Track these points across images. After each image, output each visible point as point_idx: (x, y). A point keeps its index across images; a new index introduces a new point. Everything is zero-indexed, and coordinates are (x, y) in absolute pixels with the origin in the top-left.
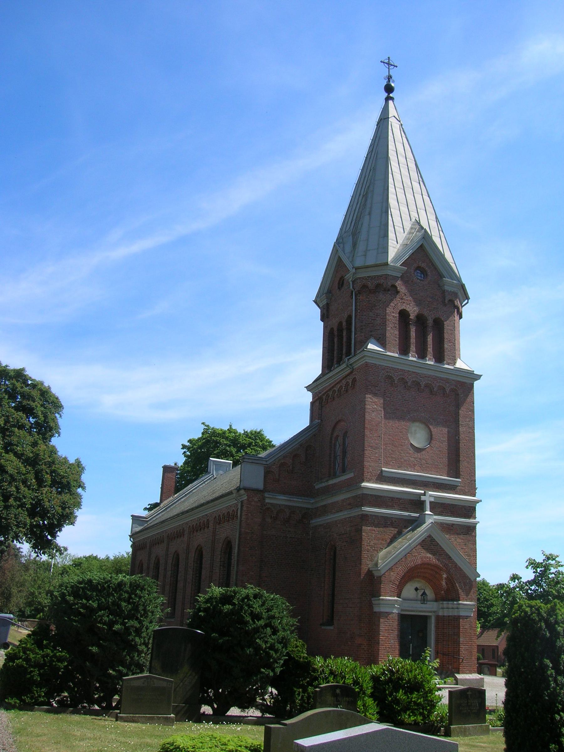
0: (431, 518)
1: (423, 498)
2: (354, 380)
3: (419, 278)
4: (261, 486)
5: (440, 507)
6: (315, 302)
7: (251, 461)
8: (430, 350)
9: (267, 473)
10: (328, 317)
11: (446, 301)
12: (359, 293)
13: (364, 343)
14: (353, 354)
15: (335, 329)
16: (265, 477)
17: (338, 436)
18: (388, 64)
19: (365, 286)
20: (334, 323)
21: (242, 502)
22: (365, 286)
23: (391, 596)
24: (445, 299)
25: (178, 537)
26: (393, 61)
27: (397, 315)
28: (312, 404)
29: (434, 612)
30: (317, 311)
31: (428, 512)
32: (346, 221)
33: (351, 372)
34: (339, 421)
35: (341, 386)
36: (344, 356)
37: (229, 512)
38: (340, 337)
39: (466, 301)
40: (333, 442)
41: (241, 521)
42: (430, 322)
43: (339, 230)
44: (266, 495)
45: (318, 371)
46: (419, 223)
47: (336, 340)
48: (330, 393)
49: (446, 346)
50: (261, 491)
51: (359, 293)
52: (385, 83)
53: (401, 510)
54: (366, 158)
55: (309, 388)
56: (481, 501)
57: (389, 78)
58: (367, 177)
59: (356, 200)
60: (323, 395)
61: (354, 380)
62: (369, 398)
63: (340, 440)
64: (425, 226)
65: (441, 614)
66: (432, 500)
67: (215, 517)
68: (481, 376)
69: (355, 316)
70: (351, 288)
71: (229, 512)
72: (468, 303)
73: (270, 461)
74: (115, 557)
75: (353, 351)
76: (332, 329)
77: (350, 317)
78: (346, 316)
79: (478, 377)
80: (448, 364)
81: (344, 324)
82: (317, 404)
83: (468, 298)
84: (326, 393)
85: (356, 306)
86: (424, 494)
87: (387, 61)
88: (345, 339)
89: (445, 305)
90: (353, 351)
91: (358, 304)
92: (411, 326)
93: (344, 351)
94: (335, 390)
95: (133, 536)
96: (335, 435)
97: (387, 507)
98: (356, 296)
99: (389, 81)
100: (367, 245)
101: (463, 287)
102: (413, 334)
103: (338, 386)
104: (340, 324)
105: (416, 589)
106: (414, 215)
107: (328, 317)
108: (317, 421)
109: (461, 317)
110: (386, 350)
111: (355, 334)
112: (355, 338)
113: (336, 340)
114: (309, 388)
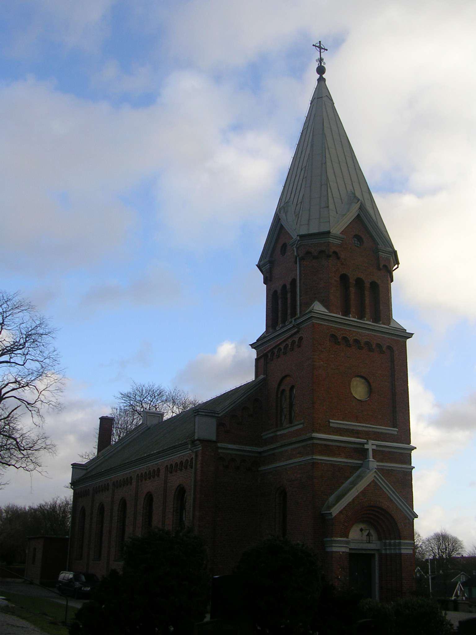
0: (373, 464)
1: (366, 446)
2: (301, 339)
4: (214, 438)
5: (380, 455)
6: (259, 266)
7: (203, 414)
8: (368, 311)
9: (220, 424)
10: (271, 281)
11: (381, 267)
12: (302, 259)
13: (309, 304)
15: (279, 291)
16: (217, 429)
17: (284, 390)
18: (320, 48)
19: (308, 253)
20: (278, 286)
21: (196, 452)
22: (308, 253)
23: (341, 537)
24: (379, 265)
25: (124, 485)
27: (338, 279)
28: (257, 360)
29: (378, 550)
30: (260, 277)
31: (371, 459)
32: (285, 193)
33: (297, 332)
34: (286, 376)
36: (289, 317)
37: (182, 461)
38: (285, 299)
39: (396, 266)
40: (279, 396)
41: (196, 470)
42: (367, 285)
44: (219, 445)
45: (264, 329)
49: (381, 307)
50: (214, 442)
51: (302, 259)
52: (316, 65)
53: (347, 458)
54: (302, 133)
55: (253, 346)
56: (416, 448)
57: (321, 60)
58: (304, 152)
59: (295, 172)
60: (268, 352)
61: (301, 339)
62: (232, 346)
63: (287, 393)
65: (383, 552)
66: (374, 447)
67: (167, 466)
69: (300, 280)
70: (295, 254)
71: (182, 461)
73: (222, 414)
74: (442, 539)
76: (275, 292)
77: (294, 282)
78: (290, 280)
81: (288, 287)
82: (262, 360)
86: (367, 443)
87: (318, 45)
89: (379, 269)
93: (289, 311)
94: (279, 348)
95: (74, 484)
96: (281, 388)
97: (334, 455)
98: (299, 262)
101: (395, 253)
102: (352, 296)
103: (290, 341)
104: (284, 286)
105: (361, 530)
106: (349, 187)
107: (271, 281)
108: (262, 377)
109: (392, 281)
111: (300, 296)
112: (300, 300)
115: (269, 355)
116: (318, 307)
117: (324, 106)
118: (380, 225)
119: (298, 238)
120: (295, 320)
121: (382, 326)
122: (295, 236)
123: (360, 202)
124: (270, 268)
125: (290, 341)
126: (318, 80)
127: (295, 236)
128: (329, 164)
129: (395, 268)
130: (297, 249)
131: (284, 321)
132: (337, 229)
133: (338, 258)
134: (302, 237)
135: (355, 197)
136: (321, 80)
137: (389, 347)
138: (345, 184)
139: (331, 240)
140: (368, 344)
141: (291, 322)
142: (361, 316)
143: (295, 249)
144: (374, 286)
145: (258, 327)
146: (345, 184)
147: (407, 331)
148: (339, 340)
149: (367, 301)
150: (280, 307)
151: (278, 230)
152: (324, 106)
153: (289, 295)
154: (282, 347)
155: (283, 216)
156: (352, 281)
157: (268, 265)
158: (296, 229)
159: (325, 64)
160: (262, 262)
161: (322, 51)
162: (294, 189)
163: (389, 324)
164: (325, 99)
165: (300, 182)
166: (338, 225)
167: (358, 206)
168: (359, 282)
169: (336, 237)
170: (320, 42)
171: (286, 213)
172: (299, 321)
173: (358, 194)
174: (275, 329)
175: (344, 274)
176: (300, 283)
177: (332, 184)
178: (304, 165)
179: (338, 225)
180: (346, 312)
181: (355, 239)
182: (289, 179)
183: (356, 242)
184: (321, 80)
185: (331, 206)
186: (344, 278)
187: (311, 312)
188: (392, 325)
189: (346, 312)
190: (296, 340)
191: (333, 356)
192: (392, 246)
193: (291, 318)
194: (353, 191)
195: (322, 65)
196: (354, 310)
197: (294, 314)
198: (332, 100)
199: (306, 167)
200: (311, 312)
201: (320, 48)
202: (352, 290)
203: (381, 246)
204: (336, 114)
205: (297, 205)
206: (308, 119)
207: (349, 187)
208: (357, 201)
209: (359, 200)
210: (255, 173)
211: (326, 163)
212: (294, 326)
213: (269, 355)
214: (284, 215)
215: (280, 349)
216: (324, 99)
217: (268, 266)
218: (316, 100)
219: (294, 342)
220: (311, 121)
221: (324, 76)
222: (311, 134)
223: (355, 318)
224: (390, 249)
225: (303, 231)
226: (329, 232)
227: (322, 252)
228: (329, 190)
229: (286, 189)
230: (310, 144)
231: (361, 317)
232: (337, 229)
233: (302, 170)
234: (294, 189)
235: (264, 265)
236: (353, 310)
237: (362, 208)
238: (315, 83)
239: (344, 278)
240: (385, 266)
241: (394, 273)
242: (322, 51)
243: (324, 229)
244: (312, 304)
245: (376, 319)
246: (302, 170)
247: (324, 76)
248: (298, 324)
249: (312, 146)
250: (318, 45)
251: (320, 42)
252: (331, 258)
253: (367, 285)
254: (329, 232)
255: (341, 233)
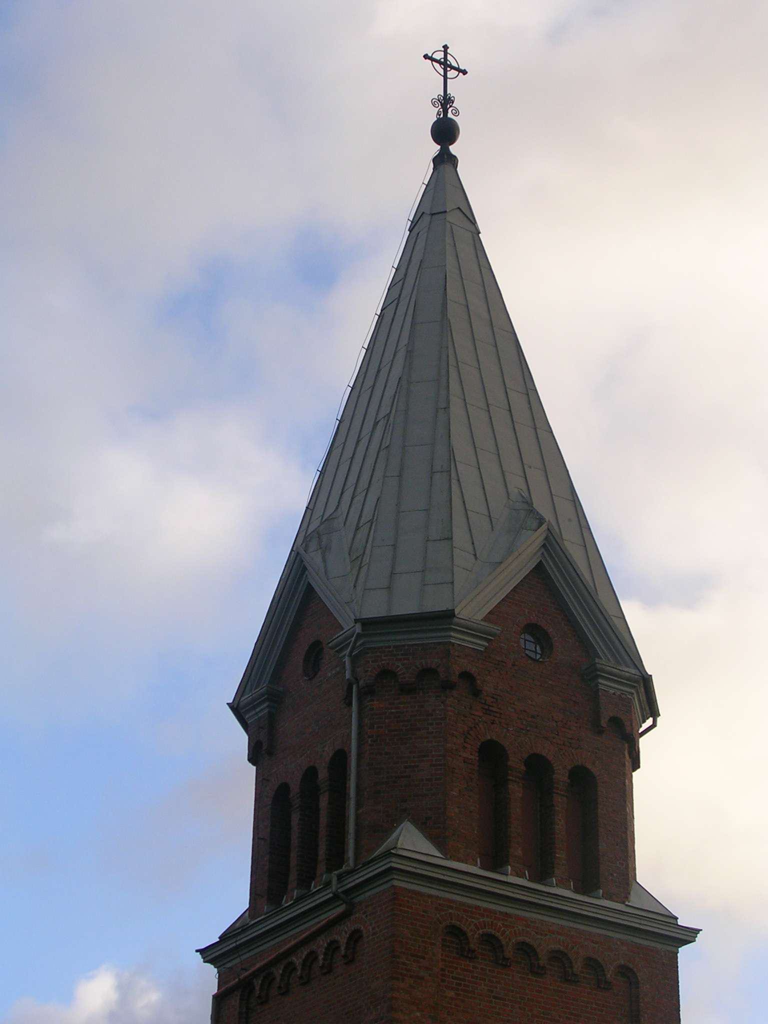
2: (356, 937)
3: (532, 655)
6: (236, 708)
8: (561, 855)
10: (270, 753)
11: (604, 723)
12: (367, 692)
13: (384, 828)
14: (351, 862)
18: (445, 64)
22: (385, 673)
26: (457, 56)
27: (474, 757)
28: (219, 1000)
30: (240, 739)
35: (312, 953)
36: (322, 867)
39: (650, 722)
43: (650, 668)
45: (243, 904)
46: (529, 503)
47: (295, 818)
48: (278, 971)
49: (602, 846)
51: (367, 692)
52: (432, 115)
55: (208, 954)
57: (446, 101)
60: (255, 975)
61: (356, 937)
64: (547, 515)
68: (697, 931)
70: (348, 675)
72: (654, 725)
75: (351, 854)
76: (284, 789)
77: (340, 759)
78: (328, 752)
79: (690, 935)
80: (608, 896)
82: (235, 1001)
83: (654, 712)
84: (260, 970)
85: (360, 726)
87: (439, 56)
88: (324, 819)
89: (600, 731)
90: (351, 854)
91: (366, 721)
92: (512, 786)
94: (291, 963)
99: (446, 112)
100: (394, 558)
101: (646, 682)
102: (516, 810)
103: (322, 943)
104: (311, 774)
106: (516, 483)
107: (270, 753)
109: (636, 765)
110: (445, 854)
111: (358, 805)
112: (357, 817)
113: (295, 818)
114: (208, 954)
115: (257, 983)
116: (411, 840)
117: (448, 240)
118: (603, 597)
119: (358, 628)
120: (340, 878)
121: (601, 904)
122: (348, 624)
123: (544, 527)
124: (271, 715)
125: (322, 943)
126: (434, 160)
127: (348, 624)
128: (456, 409)
129: (645, 726)
130: (354, 660)
131: (306, 879)
132: (473, 607)
133: (476, 693)
134: (368, 624)
135: (531, 511)
136: (445, 161)
137: (625, 972)
138: (503, 472)
139: (456, 638)
140: (558, 957)
141: (328, 884)
142: (542, 872)
143: (347, 660)
144: (582, 779)
145: (225, 894)
146: (503, 472)
147: (680, 922)
148: (472, 944)
149: (560, 825)
150: (301, 829)
151: (297, 604)
152: (448, 240)
153: (324, 802)
154: (297, 960)
155: (314, 559)
156: (515, 762)
157: (265, 703)
158: (355, 600)
159: (457, 113)
160: (246, 698)
161: (451, 73)
162: (352, 480)
163: (624, 897)
164: (454, 218)
165: (370, 461)
166: (475, 597)
167: (540, 540)
168: (538, 767)
169: (469, 630)
170: (446, 47)
171: (325, 550)
172: (351, 882)
173: (542, 507)
174: (279, 904)
175: (491, 741)
176: (358, 765)
177: (466, 471)
178: (382, 414)
179: (475, 597)
180: (495, 859)
181: (528, 637)
182: (337, 452)
183: (531, 646)
184: (445, 161)
185: (460, 535)
186: (492, 755)
187: (388, 854)
188: (634, 901)
189: (495, 859)
190: (343, 940)
191: (452, 994)
192: (636, 661)
193: (329, 870)
194: (526, 494)
195: (450, 115)
196: (519, 852)
197: (336, 858)
198: (473, 222)
199: (389, 415)
200: (388, 854)
201: (445, 64)
202: (516, 791)
203: (605, 662)
204: (482, 262)
205: (357, 528)
206: (403, 270)
207: (516, 483)
208: (535, 525)
209: (541, 521)
210: (203, 520)
211: (447, 408)
212: (336, 897)
213: (257, 983)
214: (318, 559)
215: (290, 968)
216: (449, 218)
217: (263, 710)
218: (427, 219)
219: (333, 947)
220: (410, 280)
221: (453, 149)
222: (409, 319)
223: (522, 876)
224: (633, 671)
225: (375, 608)
226: (449, 615)
227: (427, 672)
228: (455, 487)
229: (328, 479)
230: (401, 355)
231: (542, 874)
232: (473, 607)
233: (376, 423)
234: (352, 480)
235: (253, 705)
236: (517, 851)
237: (551, 545)
238: (426, 170)
239: (492, 755)
240: (616, 722)
241: (644, 743)
242: (451, 73)
243: (435, 603)
244: (392, 829)
245: (587, 883)
246: (376, 423)
247: (453, 149)
248: (347, 892)
249: (409, 353)
250: (439, 56)
251: (446, 47)
252: (454, 693)
253: (561, 776)
254: (449, 615)
255: (485, 619)
